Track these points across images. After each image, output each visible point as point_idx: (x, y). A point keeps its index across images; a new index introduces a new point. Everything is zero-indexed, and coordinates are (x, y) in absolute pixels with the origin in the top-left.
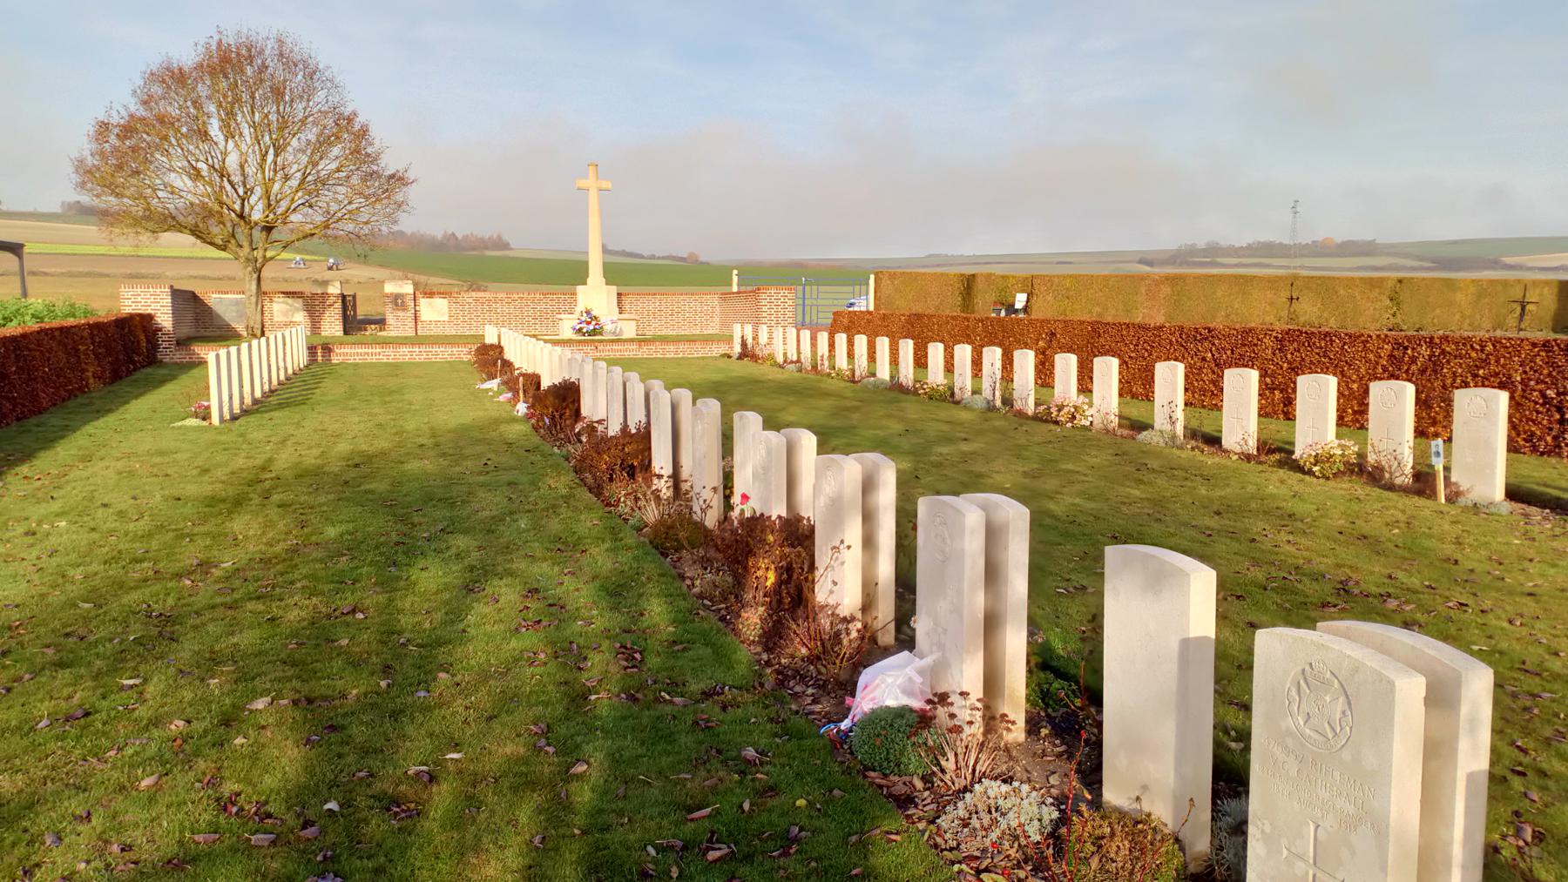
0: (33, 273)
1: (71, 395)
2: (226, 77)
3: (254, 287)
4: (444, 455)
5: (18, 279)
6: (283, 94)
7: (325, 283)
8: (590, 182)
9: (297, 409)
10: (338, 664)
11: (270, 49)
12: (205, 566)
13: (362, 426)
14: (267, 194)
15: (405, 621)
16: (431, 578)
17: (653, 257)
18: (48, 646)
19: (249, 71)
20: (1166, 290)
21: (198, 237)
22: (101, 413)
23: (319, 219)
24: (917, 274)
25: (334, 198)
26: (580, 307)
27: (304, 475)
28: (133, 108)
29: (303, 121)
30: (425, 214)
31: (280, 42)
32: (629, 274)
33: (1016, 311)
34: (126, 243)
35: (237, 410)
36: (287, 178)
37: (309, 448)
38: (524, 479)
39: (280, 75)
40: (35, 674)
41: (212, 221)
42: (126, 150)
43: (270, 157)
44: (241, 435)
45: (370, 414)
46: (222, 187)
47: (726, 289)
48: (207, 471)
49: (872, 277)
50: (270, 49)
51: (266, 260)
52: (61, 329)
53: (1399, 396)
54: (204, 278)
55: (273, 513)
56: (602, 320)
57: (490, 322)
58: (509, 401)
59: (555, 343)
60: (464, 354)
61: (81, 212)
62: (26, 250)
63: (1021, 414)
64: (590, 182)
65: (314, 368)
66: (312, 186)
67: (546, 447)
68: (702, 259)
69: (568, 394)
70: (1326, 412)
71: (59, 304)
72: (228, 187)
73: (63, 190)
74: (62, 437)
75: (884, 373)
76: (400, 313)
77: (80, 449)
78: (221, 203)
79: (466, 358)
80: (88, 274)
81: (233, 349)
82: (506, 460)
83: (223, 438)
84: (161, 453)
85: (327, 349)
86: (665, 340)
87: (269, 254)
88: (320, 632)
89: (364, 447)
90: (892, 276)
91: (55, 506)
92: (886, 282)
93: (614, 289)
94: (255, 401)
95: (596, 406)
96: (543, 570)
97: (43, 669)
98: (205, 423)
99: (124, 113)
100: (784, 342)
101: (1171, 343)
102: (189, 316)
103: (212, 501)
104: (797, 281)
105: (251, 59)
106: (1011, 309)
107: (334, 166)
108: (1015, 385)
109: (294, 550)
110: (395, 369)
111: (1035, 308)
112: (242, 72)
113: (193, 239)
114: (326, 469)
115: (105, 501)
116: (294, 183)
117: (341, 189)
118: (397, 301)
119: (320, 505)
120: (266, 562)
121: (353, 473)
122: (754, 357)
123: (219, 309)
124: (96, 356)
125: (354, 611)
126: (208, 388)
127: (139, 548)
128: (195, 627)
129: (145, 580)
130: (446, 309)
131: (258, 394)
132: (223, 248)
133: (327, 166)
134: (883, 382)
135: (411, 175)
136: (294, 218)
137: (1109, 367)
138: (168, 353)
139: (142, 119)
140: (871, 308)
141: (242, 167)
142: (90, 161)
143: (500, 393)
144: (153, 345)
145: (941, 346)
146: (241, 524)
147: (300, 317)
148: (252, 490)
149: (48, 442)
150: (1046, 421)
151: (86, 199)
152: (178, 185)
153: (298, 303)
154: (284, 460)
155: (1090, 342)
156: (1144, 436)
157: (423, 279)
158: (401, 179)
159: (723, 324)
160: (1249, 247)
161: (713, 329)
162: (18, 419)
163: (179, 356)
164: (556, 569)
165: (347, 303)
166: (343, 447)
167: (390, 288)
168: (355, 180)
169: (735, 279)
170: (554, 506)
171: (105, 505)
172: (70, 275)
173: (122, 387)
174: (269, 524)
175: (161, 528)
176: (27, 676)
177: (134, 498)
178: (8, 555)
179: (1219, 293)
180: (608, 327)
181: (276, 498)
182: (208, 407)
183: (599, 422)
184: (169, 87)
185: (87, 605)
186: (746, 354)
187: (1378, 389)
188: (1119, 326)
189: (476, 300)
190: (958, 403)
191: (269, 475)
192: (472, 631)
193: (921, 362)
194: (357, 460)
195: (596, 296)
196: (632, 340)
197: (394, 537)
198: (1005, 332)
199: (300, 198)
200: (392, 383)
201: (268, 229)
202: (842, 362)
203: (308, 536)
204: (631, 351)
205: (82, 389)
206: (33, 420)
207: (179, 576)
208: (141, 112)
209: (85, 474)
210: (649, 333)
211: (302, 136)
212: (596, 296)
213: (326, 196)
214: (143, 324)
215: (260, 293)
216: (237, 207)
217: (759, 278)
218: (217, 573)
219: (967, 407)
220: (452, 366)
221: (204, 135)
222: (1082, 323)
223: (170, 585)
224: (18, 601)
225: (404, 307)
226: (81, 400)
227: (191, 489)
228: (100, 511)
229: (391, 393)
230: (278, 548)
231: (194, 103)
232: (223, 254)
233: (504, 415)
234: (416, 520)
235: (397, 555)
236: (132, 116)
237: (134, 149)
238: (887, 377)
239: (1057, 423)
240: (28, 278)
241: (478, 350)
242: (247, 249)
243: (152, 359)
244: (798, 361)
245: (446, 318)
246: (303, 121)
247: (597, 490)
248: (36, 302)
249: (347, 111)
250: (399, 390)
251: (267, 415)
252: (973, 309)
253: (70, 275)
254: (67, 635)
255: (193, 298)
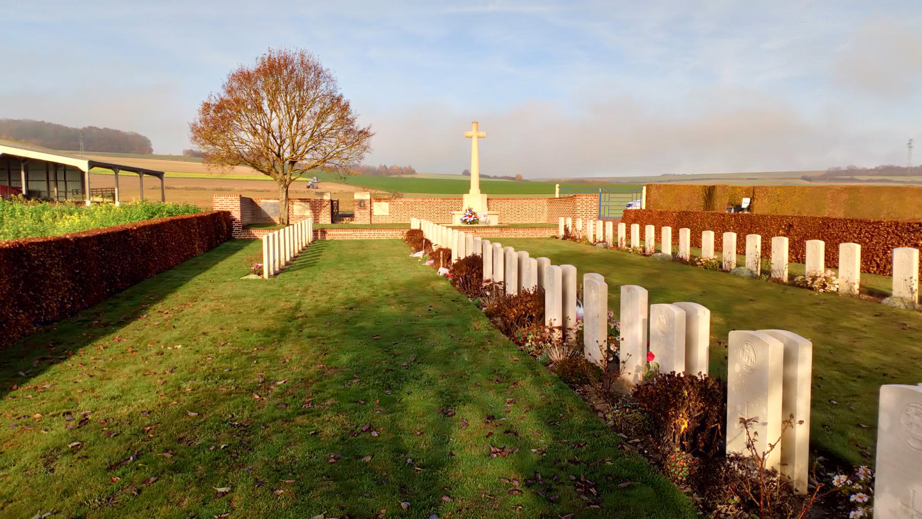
0: (168, 188)
1: (187, 258)
2: (273, 76)
3: (284, 196)
4: (402, 302)
5: (160, 191)
6: (303, 85)
7: (322, 194)
8: (473, 133)
9: (309, 269)
10: (367, 481)
11: (297, 60)
12: (267, 383)
13: (349, 281)
14: (293, 143)
15: (408, 441)
16: (418, 401)
17: (495, 177)
18: (167, 451)
19: (285, 72)
20: (845, 196)
21: (255, 168)
22: (203, 269)
23: (320, 157)
24: (675, 186)
25: (329, 144)
26: (465, 207)
27: (324, 315)
28: (222, 96)
29: (313, 101)
30: (376, 156)
31: (302, 56)
32: (493, 188)
33: (742, 209)
34: (217, 171)
35: (277, 269)
36: (304, 134)
37: (321, 295)
38: (457, 321)
39: (302, 74)
40: (158, 477)
41: (261, 159)
42: (218, 120)
43: (295, 122)
44: (281, 286)
45: (353, 273)
46: (268, 139)
47: (551, 196)
48: (263, 310)
49: (645, 188)
50: (297, 60)
51: (291, 181)
52: (183, 220)
53: (731, 236)
54: (254, 191)
55: (306, 342)
56: (479, 215)
57: (412, 216)
58: (432, 265)
59: (453, 228)
60: (399, 235)
61: (193, 155)
62: (165, 175)
63: (778, 281)
64: (473, 133)
65: (317, 243)
66: (317, 138)
67: (464, 298)
68: (525, 178)
69: (474, 264)
70: (854, 264)
71: (181, 205)
72: (272, 139)
73: (185, 143)
74: (181, 285)
75: (667, 249)
76: (362, 211)
77: (190, 293)
78: (268, 148)
79: (400, 237)
80: (195, 189)
81: (276, 233)
82: (442, 307)
83: (271, 287)
84: (236, 297)
85: (324, 232)
86: (516, 227)
87: (293, 178)
88: (349, 447)
89: (354, 296)
90: (658, 187)
91: (176, 333)
92: (653, 191)
93: (485, 196)
94: (287, 264)
95: (492, 272)
96: (491, 397)
97: (163, 472)
98: (260, 277)
99: (218, 98)
100: (594, 229)
101: (888, 233)
102: (249, 213)
103: (268, 332)
104: (596, 191)
105: (286, 67)
106: (739, 208)
107: (329, 126)
108: (773, 261)
109: (321, 373)
110: (361, 244)
111: (756, 207)
112: (281, 74)
113: (252, 169)
114: (334, 310)
115: (205, 330)
116: (308, 136)
117: (333, 140)
118: (361, 204)
119: (335, 337)
120: (306, 381)
121: (350, 314)
122: (574, 239)
123: (265, 208)
124: (200, 236)
125: (370, 429)
126: (262, 255)
127: (225, 367)
128: (264, 438)
129: (230, 394)
130: (387, 209)
131: (288, 259)
132: (268, 174)
133: (325, 126)
134: (667, 256)
135: (371, 131)
136: (307, 156)
137: (853, 251)
138: (238, 234)
139: (227, 101)
140: (644, 208)
141: (280, 127)
142: (199, 125)
143: (424, 260)
144: (230, 228)
145: (712, 233)
146: (285, 350)
147: (308, 213)
148: (290, 325)
149: (173, 288)
150: (802, 287)
151: (196, 147)
152: (245, 139)
153: (307, 205)
154: (308, 303)
155: (833, 233)
156: (886, 301)
157: (373, 191)
158: (366, 133)
159: (550, 215)
160: (876, 169)
161: (543, 220)
162: (157, 273)
163: (243, 235)
164: (501, 398)
165: (334, 205)
166: (340, 295)
167: (358, 196)
168: (341, 134)
169: (557, 190)
170: (482, 344)
171: (204, 334)
172: (186, 189)
173: (213, 253)
174: (304, 351)
175: (238, 352)
176: (153, 479)
177: (222, 329)
178: (146, 370)
179: (883, 199)
180: (482, 219)
181: (306, 331)
182: (261, 267)
183: (500, 283)
184: (242, 83)
185: (193, 414)
186: (567, 236)
187: (681, 230)
188: (844, 221)
189: (405, 203)
190: (727, 271)
191: (299, 315)
192: (458, 455)
193: (696, 243)
194: (351, 305)
195: (474, 200)
196: (496, 227)
197: (385, 365)
198: (745, 224)
199: (310, 145)
200: (361, 253)
201: (293, 163)
202: (635, 242)
203: (330, 360)
204: (496, 233)
205: (192, 255)
206: (166, 274)
207: (250, 391)
208: (227, 97)
209: (194, 310)
210: (505, 222)
211: (312, 110)
212: (474, 200)
213: (325, 143)
214: (225, 216)
215: (288, 199)
216: (276, 150)
217: (575, 189)
218: (276, 390)
219: (736, 275)
220: (394, 242)
221: (260, 110)
222: (814, 218)
223: (246, 399)
224: (150, 408)
225: (364, 207)
226: (192, 261)
227: (255, 324)
228: (202, 338)
229: (362, 259)
230: (312, 370)
231: (255, 92)
232: (269, 178)
233: (432, 275)
234: (396, 351)
235: (392, 380)
236: (222, 99)
237: (223, 118)
238: (670, 253)
239: (811, 289)
240: (165, 191)
241: (408, 233)
242: (281, 174)
243: (230, 238)
244: (604, 241)
245: (387, 214)
246: (313, 101)
247: (508, 332)
248: (169, 204)
249: (337, 95)
250: (366, 258)
251: (295, 273)
252: (710, 207)
253: (186, 189)
254: (180, 440)
255: (251, 201)
